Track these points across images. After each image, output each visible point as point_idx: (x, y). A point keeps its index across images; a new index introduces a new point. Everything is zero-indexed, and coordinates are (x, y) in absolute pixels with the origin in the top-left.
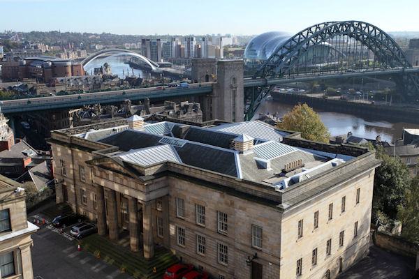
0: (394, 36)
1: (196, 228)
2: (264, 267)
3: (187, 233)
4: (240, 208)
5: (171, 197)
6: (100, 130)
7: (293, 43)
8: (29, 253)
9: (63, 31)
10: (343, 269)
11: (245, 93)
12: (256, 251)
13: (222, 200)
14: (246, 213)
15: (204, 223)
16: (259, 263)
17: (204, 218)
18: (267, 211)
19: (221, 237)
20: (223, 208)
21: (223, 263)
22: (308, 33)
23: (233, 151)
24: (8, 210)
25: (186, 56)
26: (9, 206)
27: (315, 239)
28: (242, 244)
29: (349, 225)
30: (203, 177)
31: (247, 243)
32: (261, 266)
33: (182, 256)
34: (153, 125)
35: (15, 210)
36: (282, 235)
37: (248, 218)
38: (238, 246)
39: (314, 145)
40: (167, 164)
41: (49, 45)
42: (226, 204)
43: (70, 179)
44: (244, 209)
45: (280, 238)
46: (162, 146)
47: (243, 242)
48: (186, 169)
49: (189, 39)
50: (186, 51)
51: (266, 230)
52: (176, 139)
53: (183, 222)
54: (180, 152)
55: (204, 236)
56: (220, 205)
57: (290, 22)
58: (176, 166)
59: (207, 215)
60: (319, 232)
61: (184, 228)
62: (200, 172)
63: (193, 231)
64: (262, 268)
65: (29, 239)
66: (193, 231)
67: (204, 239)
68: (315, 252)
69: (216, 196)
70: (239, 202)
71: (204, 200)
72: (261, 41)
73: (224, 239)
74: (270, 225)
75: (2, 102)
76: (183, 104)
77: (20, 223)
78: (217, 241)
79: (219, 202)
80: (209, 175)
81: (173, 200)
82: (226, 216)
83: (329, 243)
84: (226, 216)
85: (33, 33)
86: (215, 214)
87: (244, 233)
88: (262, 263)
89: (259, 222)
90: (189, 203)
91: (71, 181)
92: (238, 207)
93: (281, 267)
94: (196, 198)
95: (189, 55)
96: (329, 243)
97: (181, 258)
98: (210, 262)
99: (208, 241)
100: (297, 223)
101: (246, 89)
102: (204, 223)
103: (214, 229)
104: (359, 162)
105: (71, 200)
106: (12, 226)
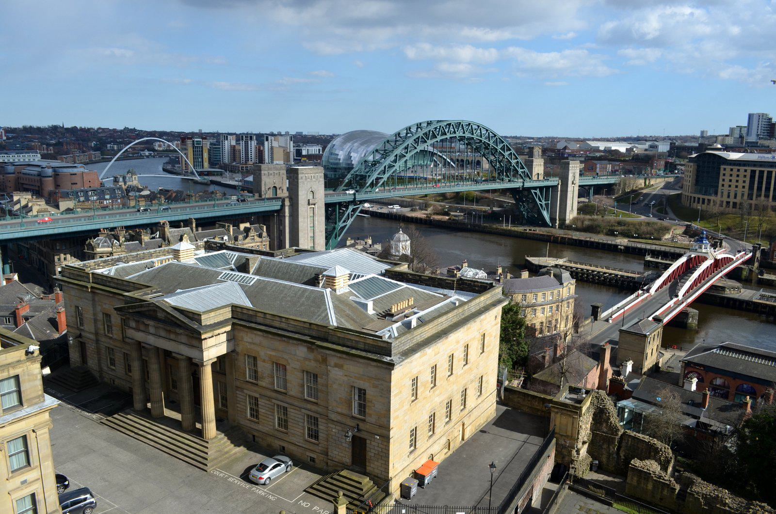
1: (274, 395)
2: (368, 442)
3: (261, 402)
4: (336, 365)
5: (237, 354)
6: (131, 264)
8: (47, 436)
9: (68, 125)
10: (466, 437)
11: (326, 211)
12: (357, 422)
13: (311, 356)
14: (342, 375)
16: (362, 436)
18: (373, 370)
19: (309, 406)
20: (312, 366)
21: (313, 441)
24: (17, 378)
25: (243, 160)
26: (17, 371)
27: (433, 400)
28: (339, 413)
29: (472, 381)
31: (345, 411)
32: (365, 440)
33: (255, 434)
35: (27, 377)
36: (392, 398)
37: (346, 378)
38: (333, 416)
39: (425, 280)
42: (316, 360)
43: (90, 333)
44: (340, 367)
47: (339, 410)
49: (324, 136)
51: (370, 393)
52: (240, 274)
53: (255, 388)
54: (250, 292)
55: (286, 405)
56: (307, 363)
57: (16, 127)
58: (245, 311)
60: (437, 392)
61: (257, 395)
63: (269, 398)
64: (366, 444)
65: (46, 416)
66: (269, 398)
67: (285, 409)
68: (432, 418)
71: (285, 357)
73: (314, 408)
74: (376, 386)
76: (242, 226)
77: (33, 395)
78: (303, 411)
79: (306, 359)
81: (241, 358)
82: (316, 376)
83: (449, 405)
84: (316, 376)
85: (55, 128)
86: (299, 374)
87: (340, 398)
88: (365, 437)
89: (362, 382)
90: (264, 361)
91: (92, 337)
92: (332, 363)
93: (391, 441)
94: (273, 353)
95: (247, 159)
96: (449, 405)
97: (254, 436)
98: (293, 439)
99: (292, 412)
100: (411, 382)
101: (328, 205)
103: (300, 395)
104: (484, 299)
105: (92, 363)
106: (24, 399)
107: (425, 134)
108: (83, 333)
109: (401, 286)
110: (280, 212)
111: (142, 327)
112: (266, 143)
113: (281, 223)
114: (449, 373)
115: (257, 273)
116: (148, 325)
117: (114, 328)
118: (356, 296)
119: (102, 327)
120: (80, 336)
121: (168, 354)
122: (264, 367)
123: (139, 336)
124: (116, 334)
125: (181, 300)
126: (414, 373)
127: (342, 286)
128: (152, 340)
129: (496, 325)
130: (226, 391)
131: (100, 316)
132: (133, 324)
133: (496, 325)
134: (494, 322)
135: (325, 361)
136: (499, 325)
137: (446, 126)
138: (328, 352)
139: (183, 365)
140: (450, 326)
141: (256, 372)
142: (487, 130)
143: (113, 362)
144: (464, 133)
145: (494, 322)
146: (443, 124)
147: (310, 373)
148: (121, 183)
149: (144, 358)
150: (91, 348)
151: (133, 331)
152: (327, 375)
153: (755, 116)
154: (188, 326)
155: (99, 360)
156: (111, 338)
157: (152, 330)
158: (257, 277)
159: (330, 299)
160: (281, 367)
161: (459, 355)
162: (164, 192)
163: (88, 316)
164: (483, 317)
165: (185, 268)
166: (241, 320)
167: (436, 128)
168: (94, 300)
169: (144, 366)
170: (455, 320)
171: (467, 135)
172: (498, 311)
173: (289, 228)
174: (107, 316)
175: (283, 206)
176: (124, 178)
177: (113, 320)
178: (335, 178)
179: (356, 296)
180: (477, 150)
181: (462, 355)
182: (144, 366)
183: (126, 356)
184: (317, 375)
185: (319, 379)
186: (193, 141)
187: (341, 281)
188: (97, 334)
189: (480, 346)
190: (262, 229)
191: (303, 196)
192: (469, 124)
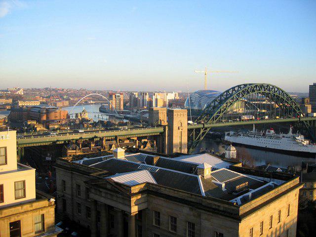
0: (286, 91)
6: (90, 159)
7: (222, 98)
15: (175, 230)
17: (175, 227)
18: (228, 222)
20: (192, 219)
22: (233, 91)
23: (196, 176)
30: (176, 195)
34: (129, 155)
40: (148, 184)
41: (43, 97)
43: (69, 195)
45: (297, 229)
46: (142, 171)
48: (162, 188)
50: (141, 102)
54: (154, 175)
58: (154, 186)
59: (178, 225)
61: (159, 234)
62: (173, 191)
69: (186, 210)
70: (205, 215)
72: (202, 94)
75: (302, 143)
76: (143, 140)
80: (181, 193)
91: (70, 197)
102: (175, 230)
107: (243, 91)
108: (65, 195)
109: (239, 175)
110: (163, 134)
111: (98, 193)
112: (154, 96)
113: (164, 140)
114: (270, 227)
115: (157, 165)
116: (101, 192)
117: (82, 192)
118: (215, 180)
119: (75, 192)
120: (63, 196)
121: (110, 208)
122: (164, 219)
123: (96, 198)
124: (83, 195)
125: (121, 179)
126: (251, 225)
127: (208, 173)
128: (102, 200)
129: (295, 200)
130: (141, 232)
131: (75, 186)
132: (93, 191)
133: (295, 200)
134: (295, 198)
135: (199, 216)
136: (298, 199)
137: (254, 87)
138: (201, 211)
139: (120, 214)
140: (271, 199)
141: (159, 221)
142: (278, 89)
143: (79, 211)
144: (265, 90)
145: (295, 198)
146: (253, 86)
147: (191, 223)
148: (79, 117)
149: (98, 210)
150: (68, 202)
151: (93, 195)
152: (201, 224)
153: (21, 141)
154: (124, 191)
155: (73, 209)
156: (80, 198)
157: (103, 195)
158: (159, 168)
159: (201, 181)
160: (174, 220)
161: (276, 216)
162: (101, 122)
163: (68, 185)
164: (289, 194)
165: (120, 162)
166: (148, 190)
167: (249, 88)
168: (72, 177)
169: (98, 214)
170: (273, 196)
171: (267, 91)
172: (297, 191)
173: (219, 127)
174: (79, 186)
175: (165, 130)
176: (81, 114)
177: (81, 188)
178: (194, 115)
179: (215, 180)
180: (272, 99)
181: (277, 217)
182: (98, 214)
183: (88, 209)
184: (194, 224)
185: (195, 226)
186: (116, 96)
187: (207, 170)
188: (72, 195)
189: (287, 212)
190: (153, 142)
191: (176, 125)
192: (268, 85)
